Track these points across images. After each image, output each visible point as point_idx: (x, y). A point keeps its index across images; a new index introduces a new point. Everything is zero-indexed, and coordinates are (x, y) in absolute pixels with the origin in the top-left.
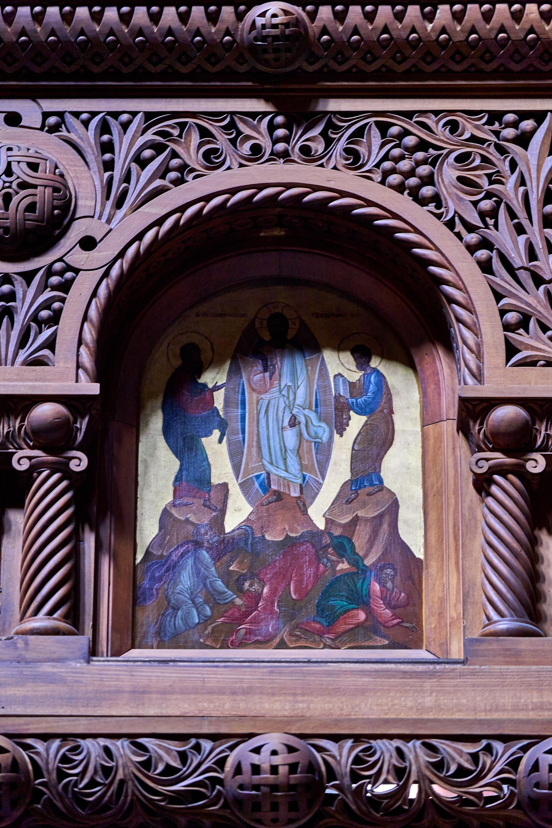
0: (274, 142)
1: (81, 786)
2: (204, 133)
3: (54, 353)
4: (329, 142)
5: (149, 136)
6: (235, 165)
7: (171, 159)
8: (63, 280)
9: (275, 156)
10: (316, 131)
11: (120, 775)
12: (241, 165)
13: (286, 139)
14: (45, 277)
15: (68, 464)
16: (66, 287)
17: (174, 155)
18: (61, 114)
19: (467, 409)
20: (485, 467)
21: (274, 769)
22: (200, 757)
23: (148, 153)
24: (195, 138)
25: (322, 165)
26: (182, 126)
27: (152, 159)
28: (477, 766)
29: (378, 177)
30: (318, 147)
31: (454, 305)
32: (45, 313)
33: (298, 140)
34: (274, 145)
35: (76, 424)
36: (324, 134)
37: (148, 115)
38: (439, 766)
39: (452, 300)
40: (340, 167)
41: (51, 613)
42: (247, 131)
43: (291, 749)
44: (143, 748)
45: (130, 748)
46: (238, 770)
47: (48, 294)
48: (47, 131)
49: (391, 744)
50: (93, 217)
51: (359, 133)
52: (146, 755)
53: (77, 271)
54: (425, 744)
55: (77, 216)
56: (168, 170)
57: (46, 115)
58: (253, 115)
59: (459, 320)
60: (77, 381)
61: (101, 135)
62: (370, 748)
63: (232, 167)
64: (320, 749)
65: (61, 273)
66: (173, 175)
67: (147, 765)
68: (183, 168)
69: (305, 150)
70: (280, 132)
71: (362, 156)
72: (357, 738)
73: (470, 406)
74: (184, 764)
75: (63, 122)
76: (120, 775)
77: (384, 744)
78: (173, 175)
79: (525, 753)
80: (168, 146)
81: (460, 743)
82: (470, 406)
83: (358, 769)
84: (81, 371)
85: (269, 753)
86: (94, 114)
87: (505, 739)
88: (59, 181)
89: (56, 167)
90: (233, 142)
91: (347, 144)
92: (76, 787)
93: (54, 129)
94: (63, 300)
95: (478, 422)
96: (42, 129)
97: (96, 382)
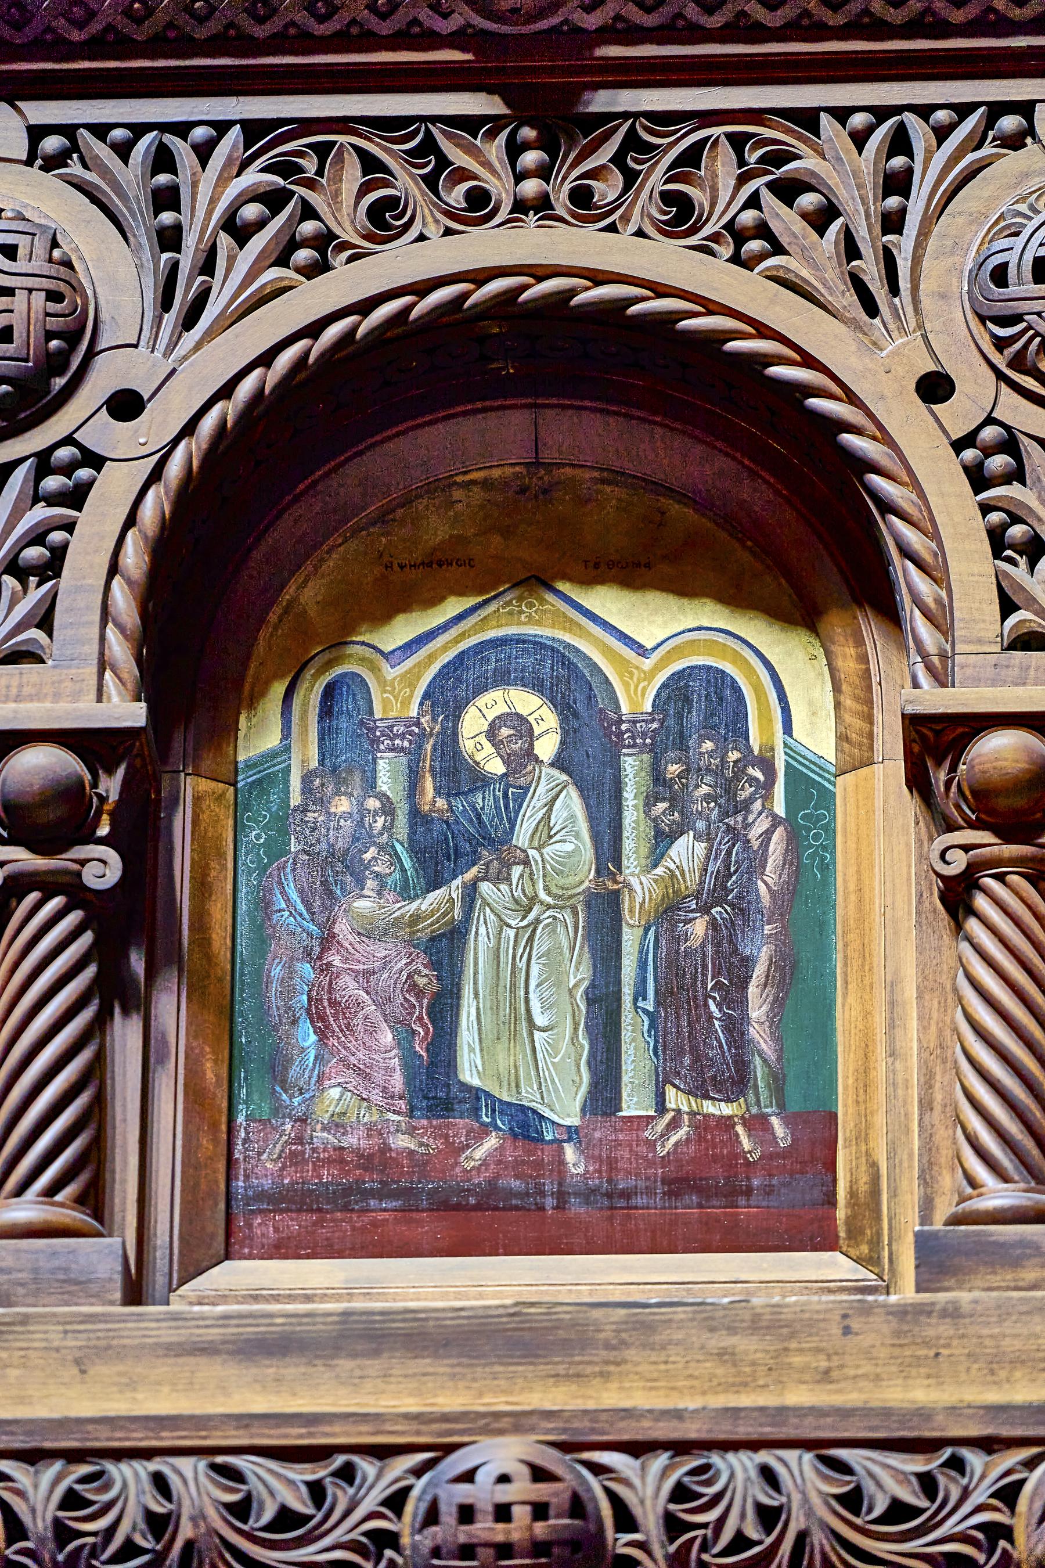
0: (519, 177)
1: (716, 1550)
2: (370, 163)
3: (50, 635)
4: (630, 178)
5: (253, 177)
6: (433, 231)
7: (301, 221)
8: (71, 483)
9: (521, 206)
10: (604, 156)
11: (186, 1531)
12: (448, 232)
13: (544, 172)
14: (32, 477)
15: (79, 874)
16: (76, 497)
17: (308, 212)
18: (68, 131)
19: (923, 737)
20: (959, 862)
21: (503, 1513)
22: (351, 1491)
23: (251, 211)
24: (353, 175)
25: (612, 228)
26: (322, 150)
27: (260, 224)
28: (933, 1500)
29: (726, 251)
30: (607, 190)
31: (894, 519)
32: (34, 553)
33: (564, 179)
34: (516, 184)
35: (96, 788)
36: (618, 160)
37: (253, 129)
38: (853, 1500)
39: (887, 507)
40: (650, 230)
41: (51, 1191)
42: (459, 158)
43: (539, 1474)
44: (235, 1475)
45: (208, 1476)
46: (432, 1516)
47: (41, 512)
48: (41, 168)
49: (751, 1459)
50: (136, 346)
51: (692, 157)
52: (238, 1491)
53: (97, 462)
54: (214, 1467)
55: (102, 345)
56: (293, 245)
57: (36, 133)
58: (469, 124)
59: (907, 553)
60: (99, 699)
61: (154, 173)
62: (705, 1468)
63: (427, 234)
64: (598, 1469)
65: (67, 470)
66: (303, 255)
67: (241, 1510)
68: (324, 241)
69: (581, 197)
70: (531, 158)
71: (697, 205)
72: (680, 1448)
73: (930, 734)
74: (319, 1505)
75: (75, 147)
76: (186, 1531)
77: (740, 1460)
78: (303, 255)
79: (1031, 1471)
80: (293, 193)
81: (895, 1455)
82: (930, 734)
83: (70, 1518)
84: (108, 675)
85: (492, 1478)
86: (139, 130)
87: (989, 1445)
88: (53, 274)
89: (55, 244)
90: (431, 181)
91: (664, 184)
92: (96, 1558)
93: (53, 163)
94: (69, 527)
95: (947, 764)
96: (29, 162)
97: (139, 700)
